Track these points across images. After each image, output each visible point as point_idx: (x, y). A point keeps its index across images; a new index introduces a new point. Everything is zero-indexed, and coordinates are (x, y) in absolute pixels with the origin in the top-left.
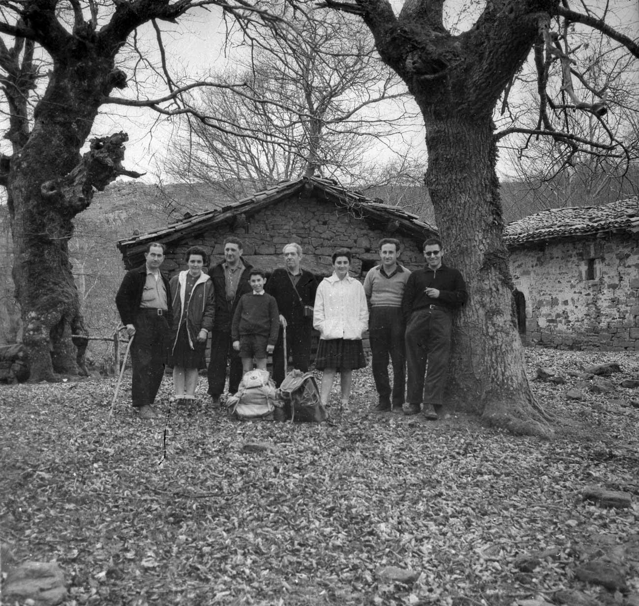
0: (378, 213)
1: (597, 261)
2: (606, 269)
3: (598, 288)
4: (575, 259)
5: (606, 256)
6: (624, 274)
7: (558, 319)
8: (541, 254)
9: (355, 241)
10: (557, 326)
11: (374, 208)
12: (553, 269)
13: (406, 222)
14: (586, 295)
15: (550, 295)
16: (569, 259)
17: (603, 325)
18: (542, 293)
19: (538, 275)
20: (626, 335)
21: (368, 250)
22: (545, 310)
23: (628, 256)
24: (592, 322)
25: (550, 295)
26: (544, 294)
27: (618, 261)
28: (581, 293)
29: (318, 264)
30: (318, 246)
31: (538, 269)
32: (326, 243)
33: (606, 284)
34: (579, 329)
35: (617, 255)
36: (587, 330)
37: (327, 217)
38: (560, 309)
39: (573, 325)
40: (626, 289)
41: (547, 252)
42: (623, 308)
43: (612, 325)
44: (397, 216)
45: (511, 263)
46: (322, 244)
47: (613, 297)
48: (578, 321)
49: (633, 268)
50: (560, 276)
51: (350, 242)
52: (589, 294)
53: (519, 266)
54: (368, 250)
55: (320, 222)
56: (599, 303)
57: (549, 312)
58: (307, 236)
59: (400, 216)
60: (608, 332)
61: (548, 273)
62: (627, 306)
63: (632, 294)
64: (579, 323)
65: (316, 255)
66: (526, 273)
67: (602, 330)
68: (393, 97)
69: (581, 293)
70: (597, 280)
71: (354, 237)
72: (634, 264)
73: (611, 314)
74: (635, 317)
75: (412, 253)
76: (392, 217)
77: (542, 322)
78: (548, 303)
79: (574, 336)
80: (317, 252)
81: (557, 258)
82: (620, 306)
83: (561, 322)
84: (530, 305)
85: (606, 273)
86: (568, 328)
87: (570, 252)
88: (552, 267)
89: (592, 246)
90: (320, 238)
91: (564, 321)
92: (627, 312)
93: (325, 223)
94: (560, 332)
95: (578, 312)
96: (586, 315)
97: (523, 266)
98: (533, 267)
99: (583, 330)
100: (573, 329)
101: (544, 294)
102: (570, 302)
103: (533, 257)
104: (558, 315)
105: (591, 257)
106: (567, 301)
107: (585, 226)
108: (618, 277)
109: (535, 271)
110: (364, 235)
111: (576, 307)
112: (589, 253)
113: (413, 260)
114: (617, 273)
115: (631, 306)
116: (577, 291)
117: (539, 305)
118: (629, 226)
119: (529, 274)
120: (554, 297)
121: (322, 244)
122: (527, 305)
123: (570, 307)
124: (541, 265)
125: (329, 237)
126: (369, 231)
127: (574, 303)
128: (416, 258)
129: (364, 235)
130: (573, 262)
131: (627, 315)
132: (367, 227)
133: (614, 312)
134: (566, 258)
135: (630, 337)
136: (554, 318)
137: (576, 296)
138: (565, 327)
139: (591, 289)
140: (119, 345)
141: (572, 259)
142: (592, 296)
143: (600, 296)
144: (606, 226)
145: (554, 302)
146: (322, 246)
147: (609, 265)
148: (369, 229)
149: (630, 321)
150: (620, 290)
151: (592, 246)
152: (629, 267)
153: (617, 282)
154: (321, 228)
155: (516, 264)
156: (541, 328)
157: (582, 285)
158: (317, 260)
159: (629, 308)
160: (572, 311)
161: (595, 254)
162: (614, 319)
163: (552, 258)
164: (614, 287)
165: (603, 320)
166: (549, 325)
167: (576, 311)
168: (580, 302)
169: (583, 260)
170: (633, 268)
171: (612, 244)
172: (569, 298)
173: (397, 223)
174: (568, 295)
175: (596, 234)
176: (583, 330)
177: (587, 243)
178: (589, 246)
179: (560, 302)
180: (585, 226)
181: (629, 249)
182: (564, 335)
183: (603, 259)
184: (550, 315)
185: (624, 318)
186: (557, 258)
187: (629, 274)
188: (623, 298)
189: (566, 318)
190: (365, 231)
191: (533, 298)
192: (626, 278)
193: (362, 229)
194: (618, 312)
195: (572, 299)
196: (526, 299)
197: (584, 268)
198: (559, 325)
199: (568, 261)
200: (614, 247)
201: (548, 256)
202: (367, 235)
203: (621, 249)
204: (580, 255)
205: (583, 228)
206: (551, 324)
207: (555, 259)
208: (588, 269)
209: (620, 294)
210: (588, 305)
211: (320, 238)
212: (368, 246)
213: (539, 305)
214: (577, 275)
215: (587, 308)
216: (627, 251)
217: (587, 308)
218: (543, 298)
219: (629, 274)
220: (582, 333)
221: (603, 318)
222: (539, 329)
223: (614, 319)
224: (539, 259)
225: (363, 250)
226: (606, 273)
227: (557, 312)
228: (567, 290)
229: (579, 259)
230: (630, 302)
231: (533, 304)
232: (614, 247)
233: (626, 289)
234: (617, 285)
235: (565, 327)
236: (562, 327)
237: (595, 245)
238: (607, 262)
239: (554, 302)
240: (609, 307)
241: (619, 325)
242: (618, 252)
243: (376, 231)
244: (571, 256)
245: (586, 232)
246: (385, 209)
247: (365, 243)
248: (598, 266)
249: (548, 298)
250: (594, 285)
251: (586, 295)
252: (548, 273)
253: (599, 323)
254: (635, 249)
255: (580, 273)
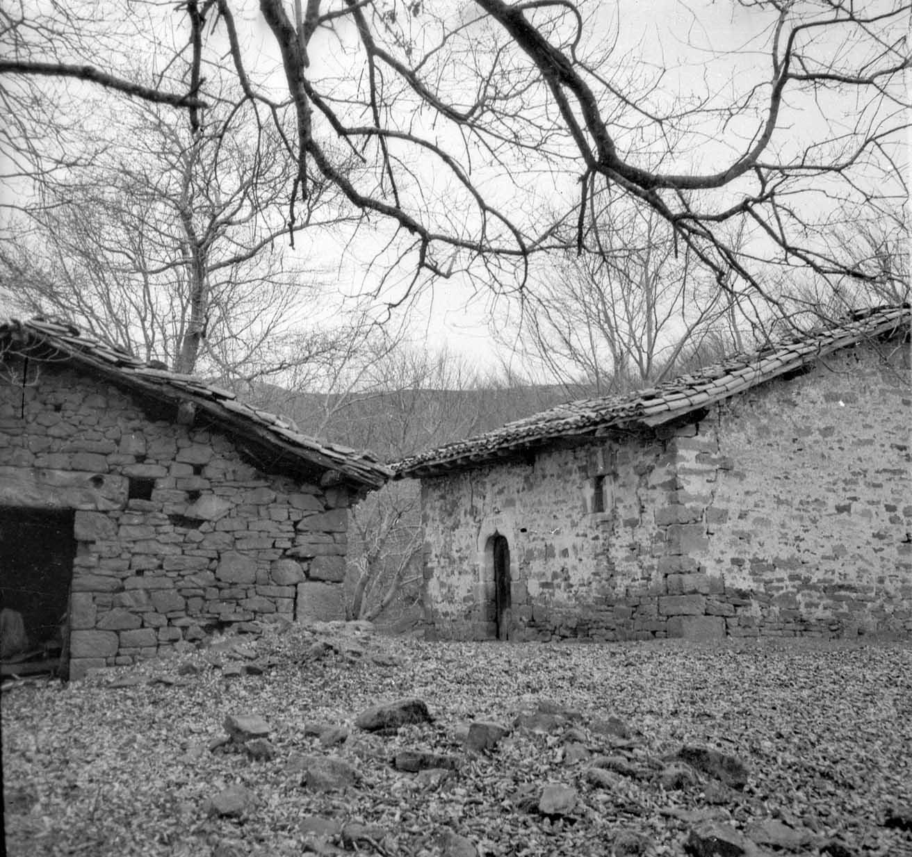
0: (155, 387)
1: (607, 479)
2: (620, 493)
3: (609, 525)
4: (576, 476)
5: (620, 470)
6: (646, 500)
7: (556, 582)
8: (529, 469)
9: (118, 442)
10: (552, 595)
11: (146, 378)
12: (546, 493)
13: (209, 405)
14: (593, 539)
15: (543, 539)
16: (567, 477)
17: (621, 590)
18: (531, 538)
19: (525, 506)
20: (653, 607)
21: (141, 459)
22: (536, 566)
23: (651, 469)
24: (603, 587)
25: (543, 539)
26: (534, 539)
27: (637, 479)
28: (586, 536)
29: (39, 486)
30: (42, 451)
31: (529, 497)
32: (57, 444)
33: (621, 520)
34: (585, 598)
35: (635, 467)
36: (597, 601)
37: (62, 396)
38: (557, 563)
39: (576, 592)
40: (650, 527)
41: (537, 465)
42: (647, 561)
43: (632, 590)
44: (190, 393)
45: (488, 486)
46: (49, 447)
47: (632, 542)
48: (583, 585)
49: (659, 489)
50: (555, 508)
51: (106, 444)
52: (596, 538)
53: (501, 492)
54: (141, 459)
55: (50, 407)
56: (613, 552)
57: (542, 570)
58: (19, 431)
59: (196, 394)
60: (627, 603)
61: (540, 503)
62: (653, 557)
63: (659, 536)
64: (584, 589)
65: (36, 469)
66: (510, 503)
67: (619, 601)
68: (320, 224)
69: (586, 536)
70: (608, 512)
71: (113, 433)
72: (660, 482)
73: (629, 572)
74: (666, 575)
75: (229, 463)
76: (182, 395)
77: (534, 588)
78: (540, 552)
79: (578, 610)
80: (39, 463)
81: (552, 475)
82: (641, 558)
83: (559, 587)
84: (516, 558)
85: (619, 500)
86: (569, 597)
87: (570, 465)
88: (544, 493)
89: (600, 454)
90: (47, 436)
91: (563, 584)
92: (652, 568)
93: (58, 408)
94: (559, 605)
95: (582, 570)
96: (595, 574)
97: (506, 491)
98: (518, 492)
99: (590, 601)
100: (577, 599)
101: (534, 539)
102: (570, 552)
103: (519, 475)
104: (555, 575)
105: (599, 473)
106: (566, 550)
107: (579, 418)
108: (639, 507)
109: (521, 500)
110: (135, 430)
111: (581, 560)
112: (595, 465)
113: (230, 476)
114: (636, 499)
115: (659, 557)
116: (581, 532)
117: (529, 557)
118: (641, 414)
119: (514, 505)
120: (548, 543)
121: (49, 447)
122: (511, 557)
123: (571, 561)
124: (531, 487)
125: (64, 434)
126: (146, 423)
127: (576, 553)
128: (234, 472)
129: (135, 430)
130: (574, 482)
131: (654, 573)
132: (142, 415)
133: (634, 568)
134: (564, 475)
135: (660, 614)
136: (549, 581)
137: (579, 541)
138: (565, 595)
139: (601, 528)
140: (852, 583)
141: (572, 478)
142: (601, 541)
143: (613, 540)
144: (607, 417)
145: (549, 553)
146: (49, 451)
147: (624, 485)
148: (145, 419)
149: (658, 582)
150: (642, 530)
151: (600, 454)
152: (654, 487)
153: (637, 516)
154: (50, 417)
155: (496, 489)
156: (532, 598)
157: (587, 521)
158: (37, 476)
159: (655, 561)
160: (574, 568)
161: (605, 466)
162: (634, 580)
163: (544, 477)
164: (632, 524)
165: (619, 582)
166: (542, 593)
167: (580, 566)
168: (586, 552)
169: (588, 478)
170: (659, 489)
171: (628, 449)
172: (568, 545)
173: (190, 408)
174: (567, 539)
175: (594, 431)
176: (590, 601)
177: (593, 449)
178: (595, 453)
179: (557, 552)
180: (579, 418)
181: (653, 457)
182: (563, 610)
183: (615, 475)
184: (544, 574)
185: (649, 579)
186: (552, 475)
187: (653, 501)
188: (646, 544)
189: (566, 579)
190: (136, 423)
191: (520, 546)
192: (649, 508)
193: (130, 419)
194: (641, 567)
195: (574, 547)
196: (510, 547)
197: (589, 492)
198: (557, 590)
199: (566, 481)
200: (630, 455)
201: (539, 473)
202: (141, 430)
203: (641, 458)
204: (583, 469)
205: (576, 422)
206: (546, 590)
207: (548, 477)
208: (596, 494)
209: (643, 536)
210: (596, 555)
211: (47, 436)
212: (142, 451)
213: (529, 557)
214: (579, 503)
215: (595, 562)
216: (649, 460)
217: (595, 562)
218: (532, 546)
219: (653, 501)
220: (589, 606)
221: (618, 579)
222: (529, 600)
223: (634, 580)
224: (527, 479)
225: (131, 459)
226: (619, 500)
227: (553, 569)
228: (566, 531)
229: (582, 478)
230: (656, 551)
231: (520, 556)
232: (630, 455)
233: (650, 527)
234: (637, 521)
235: (565, 595)
236: (561, 595)
237: (603, 450)
238: (620, 481)
239: (549, 553)
240: (627, 559)
241: (640, 591)
242: (636, 463)
243: (159, 423)
244: (570, 473)
245: (581, 428)
246: (168, 382)
247: (135, 444)
248: (609, 488)
249: (540, 545)
250: (604, 522)
251: (593, 539)
252: (540, 503)
253: (614, 588)
254: (661, 457)
255: (584, 500)
